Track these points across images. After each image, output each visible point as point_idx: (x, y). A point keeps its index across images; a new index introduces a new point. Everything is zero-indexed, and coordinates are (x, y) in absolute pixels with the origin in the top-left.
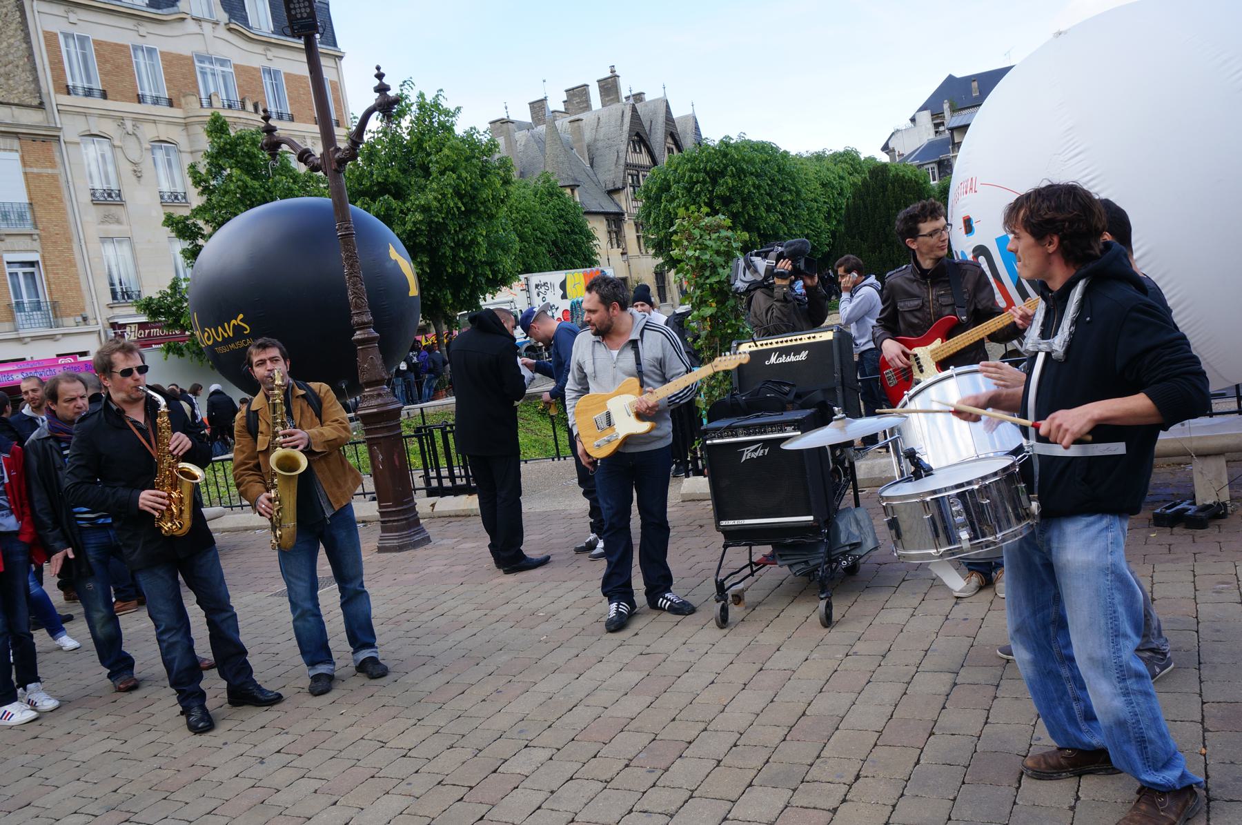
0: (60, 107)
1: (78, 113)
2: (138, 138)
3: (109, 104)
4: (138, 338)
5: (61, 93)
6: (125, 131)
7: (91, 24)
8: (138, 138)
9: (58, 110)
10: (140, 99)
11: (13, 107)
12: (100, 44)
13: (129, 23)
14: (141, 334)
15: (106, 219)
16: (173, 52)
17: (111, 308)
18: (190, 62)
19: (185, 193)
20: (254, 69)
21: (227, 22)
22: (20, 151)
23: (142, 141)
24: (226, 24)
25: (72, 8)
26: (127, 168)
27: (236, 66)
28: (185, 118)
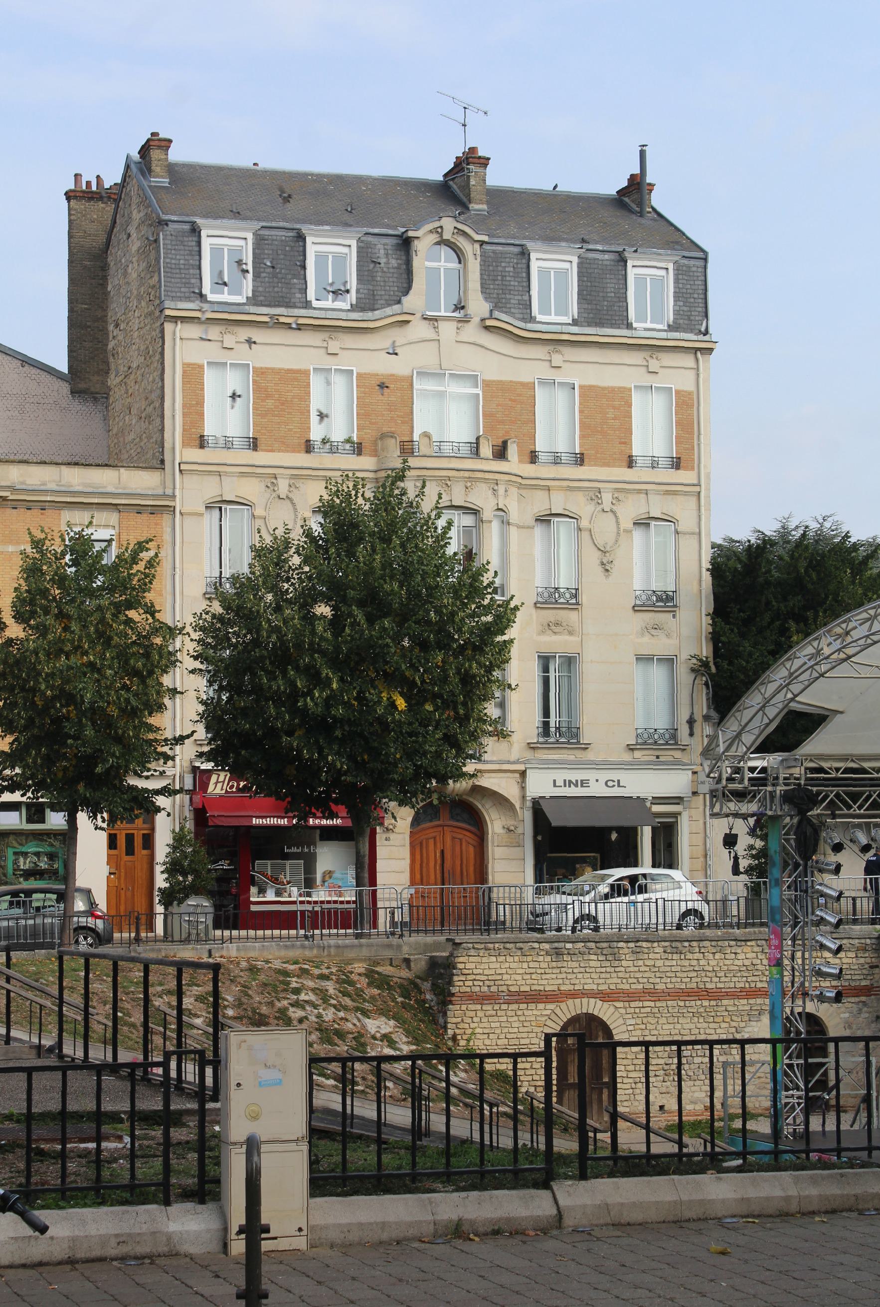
0: (183, 467)
1: (639, 491)
2: (293, 504)
3: (261, 458)
4: (227, 792)
5: (191, 447)
6: (274, 495)
7: (300, 348)
8: (293, 504)
9: (181, 471)
10: (308, 447)
11: (63, 468)
12: (263, 373)
13: (636, 358)
14: (232, 787)
15: (551, 627)
16: (380, 373)
17: (632, 750)
18: (406, 385)
19: (577, 589)
20: (523, 384)
21: (487, 315)
22: (117, 528)
23: (298, 507)
24: (483, 320)
25: (230, 328)
26: (592, 557)
27: (487, 384)
28: (376, 472)
